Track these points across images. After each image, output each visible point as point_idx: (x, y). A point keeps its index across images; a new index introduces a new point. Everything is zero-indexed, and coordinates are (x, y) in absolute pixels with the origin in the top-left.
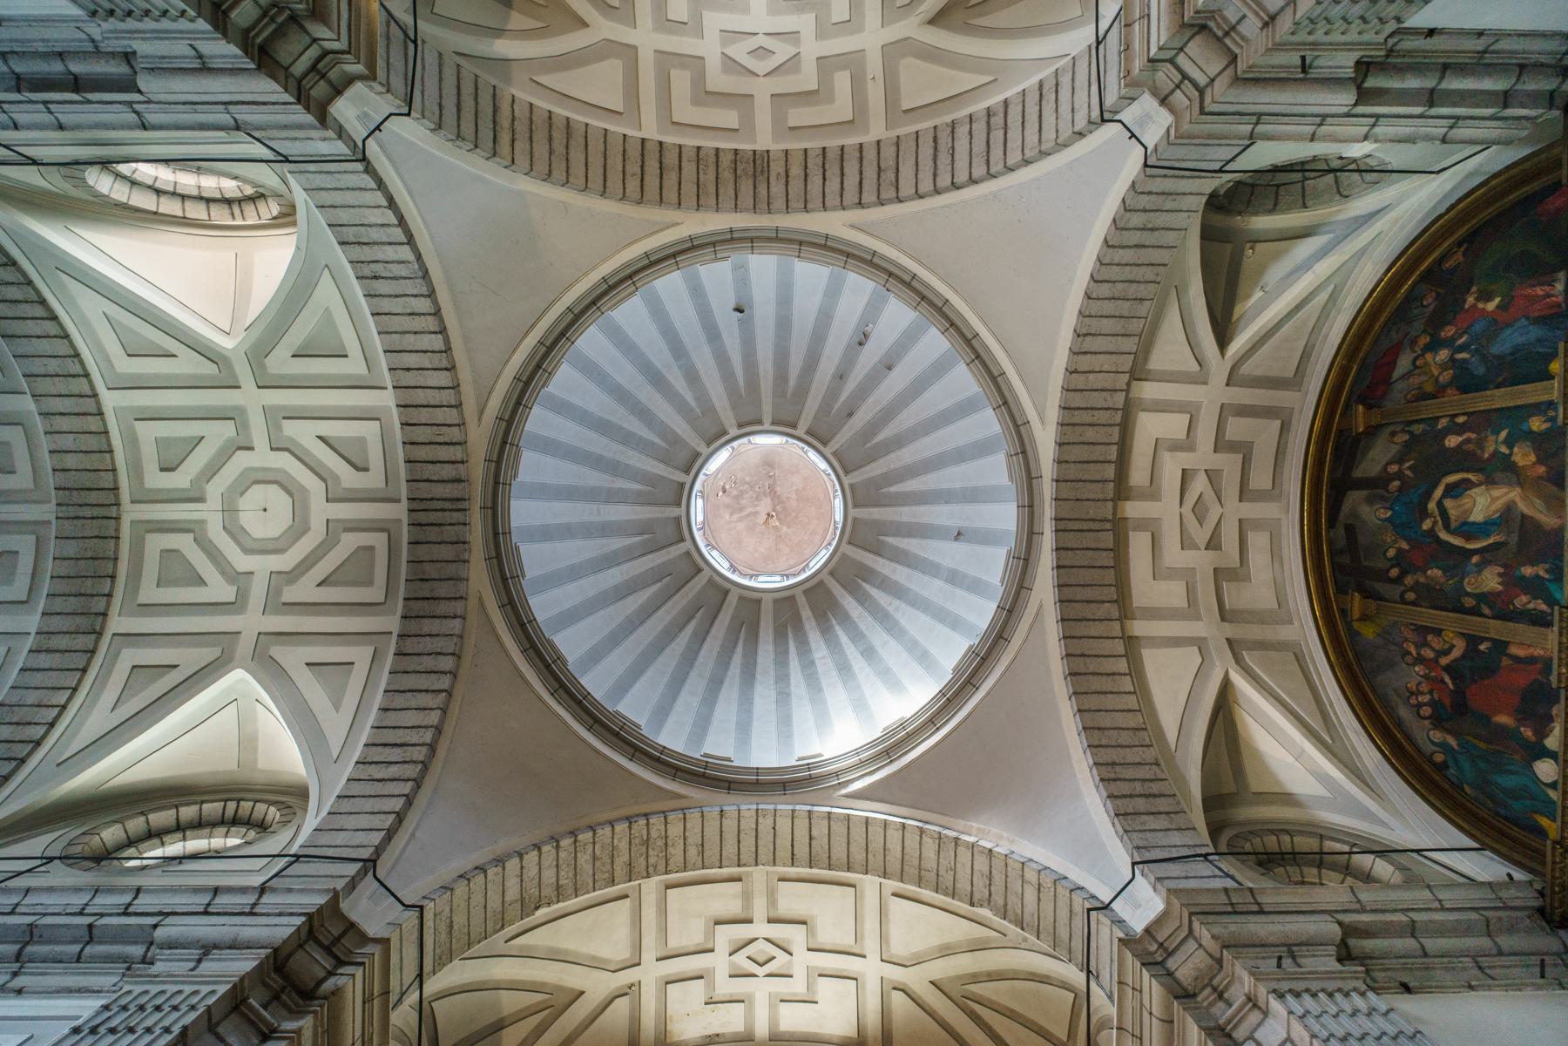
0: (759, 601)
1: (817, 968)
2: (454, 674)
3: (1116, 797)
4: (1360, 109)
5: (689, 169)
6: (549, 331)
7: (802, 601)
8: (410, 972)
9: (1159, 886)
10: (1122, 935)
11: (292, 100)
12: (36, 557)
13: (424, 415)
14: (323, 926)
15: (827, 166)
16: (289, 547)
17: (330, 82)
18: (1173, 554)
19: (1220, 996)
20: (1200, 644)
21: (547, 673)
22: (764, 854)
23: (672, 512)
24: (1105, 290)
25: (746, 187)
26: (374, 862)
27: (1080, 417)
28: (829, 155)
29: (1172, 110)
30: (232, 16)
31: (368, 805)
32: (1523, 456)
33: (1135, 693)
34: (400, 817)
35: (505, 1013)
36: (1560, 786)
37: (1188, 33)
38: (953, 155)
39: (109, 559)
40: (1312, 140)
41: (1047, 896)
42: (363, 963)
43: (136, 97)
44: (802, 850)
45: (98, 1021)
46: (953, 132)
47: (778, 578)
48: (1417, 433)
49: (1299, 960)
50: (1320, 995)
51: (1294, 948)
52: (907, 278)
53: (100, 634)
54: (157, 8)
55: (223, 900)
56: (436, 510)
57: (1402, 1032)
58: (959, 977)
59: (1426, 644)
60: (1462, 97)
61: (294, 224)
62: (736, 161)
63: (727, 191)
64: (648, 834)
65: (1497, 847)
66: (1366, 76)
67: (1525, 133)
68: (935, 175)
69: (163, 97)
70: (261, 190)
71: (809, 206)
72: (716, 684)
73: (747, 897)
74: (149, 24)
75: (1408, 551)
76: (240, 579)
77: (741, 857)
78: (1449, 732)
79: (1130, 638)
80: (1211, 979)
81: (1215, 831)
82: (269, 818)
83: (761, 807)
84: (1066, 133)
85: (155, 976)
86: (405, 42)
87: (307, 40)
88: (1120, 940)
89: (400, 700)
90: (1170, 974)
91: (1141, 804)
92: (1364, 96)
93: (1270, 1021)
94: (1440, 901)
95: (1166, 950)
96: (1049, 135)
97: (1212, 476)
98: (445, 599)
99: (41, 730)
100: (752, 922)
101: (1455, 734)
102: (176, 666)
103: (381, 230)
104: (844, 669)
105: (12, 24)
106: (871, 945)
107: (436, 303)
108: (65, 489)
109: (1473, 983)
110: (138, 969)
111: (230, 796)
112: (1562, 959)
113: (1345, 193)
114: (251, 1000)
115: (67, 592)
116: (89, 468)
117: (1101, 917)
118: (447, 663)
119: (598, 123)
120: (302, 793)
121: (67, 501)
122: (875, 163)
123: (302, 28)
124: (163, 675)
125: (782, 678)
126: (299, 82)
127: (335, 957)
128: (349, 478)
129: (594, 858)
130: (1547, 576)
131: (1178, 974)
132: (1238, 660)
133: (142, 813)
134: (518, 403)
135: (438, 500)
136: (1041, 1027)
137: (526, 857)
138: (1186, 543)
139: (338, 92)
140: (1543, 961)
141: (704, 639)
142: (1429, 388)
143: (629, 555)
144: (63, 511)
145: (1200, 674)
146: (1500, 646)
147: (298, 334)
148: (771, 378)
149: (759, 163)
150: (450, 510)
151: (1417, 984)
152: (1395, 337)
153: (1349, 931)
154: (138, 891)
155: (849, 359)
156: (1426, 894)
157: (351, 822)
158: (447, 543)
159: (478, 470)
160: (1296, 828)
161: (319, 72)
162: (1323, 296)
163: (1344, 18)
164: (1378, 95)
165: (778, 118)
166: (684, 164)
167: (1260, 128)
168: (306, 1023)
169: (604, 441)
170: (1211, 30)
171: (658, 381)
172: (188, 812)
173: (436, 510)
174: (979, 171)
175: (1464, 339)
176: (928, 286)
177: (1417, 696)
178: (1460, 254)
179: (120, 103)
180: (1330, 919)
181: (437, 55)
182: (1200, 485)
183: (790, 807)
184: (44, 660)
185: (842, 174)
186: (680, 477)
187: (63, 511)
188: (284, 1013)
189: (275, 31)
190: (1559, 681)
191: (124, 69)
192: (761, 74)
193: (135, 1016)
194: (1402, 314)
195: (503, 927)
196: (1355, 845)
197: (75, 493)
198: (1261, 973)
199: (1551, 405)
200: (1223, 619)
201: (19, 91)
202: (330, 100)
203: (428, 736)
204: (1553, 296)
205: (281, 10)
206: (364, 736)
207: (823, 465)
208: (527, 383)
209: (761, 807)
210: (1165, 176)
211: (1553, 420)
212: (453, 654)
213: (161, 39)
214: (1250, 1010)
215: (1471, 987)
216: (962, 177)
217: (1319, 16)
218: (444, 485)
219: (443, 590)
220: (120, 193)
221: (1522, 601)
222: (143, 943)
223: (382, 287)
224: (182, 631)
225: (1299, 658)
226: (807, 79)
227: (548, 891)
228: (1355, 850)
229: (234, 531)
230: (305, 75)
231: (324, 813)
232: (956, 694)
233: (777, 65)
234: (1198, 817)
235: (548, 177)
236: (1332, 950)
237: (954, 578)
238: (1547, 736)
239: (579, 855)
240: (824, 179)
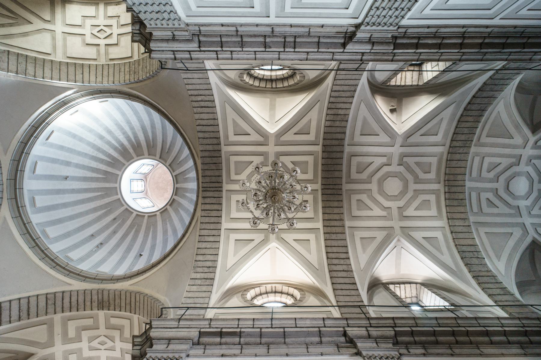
1: (82, 28)
5: (123, 304)
13: (213, 220)
15: (77, 305)
22: (100, 69)
25: (106, 298)
28: (76, 309)
38: (20, 309)
44: (86, 70)
52: (58, 267)
56: (212, 187)
62: (109, 307)
64: (134, 76)
71: (83, 292)
73: (107, 53)
77: (108, 67)
98: (207, 157)
100: (105, 45)
102: (295, 134)
105: (217, 355)
106: (59, 37)
108: (339, 194)
115: (336, 159)
116: (330, 202)
121: (338, 190)
124: (299, 131)
128: (364, 197)
129: (146, 67)
135: (212, 191)
144: (340, 187)
149: (101, 306)
150: (207, 187)
158: (208, 176)
166: (124, 306)
173: (212, 187)
185: (70, 302)
187: (340, 187)
192: (102, 336)
197: (335, 193)
218: (209, 196)
224: (296, 146)
226: (85, 335)
233: (97, 339)
240: (77, 301)
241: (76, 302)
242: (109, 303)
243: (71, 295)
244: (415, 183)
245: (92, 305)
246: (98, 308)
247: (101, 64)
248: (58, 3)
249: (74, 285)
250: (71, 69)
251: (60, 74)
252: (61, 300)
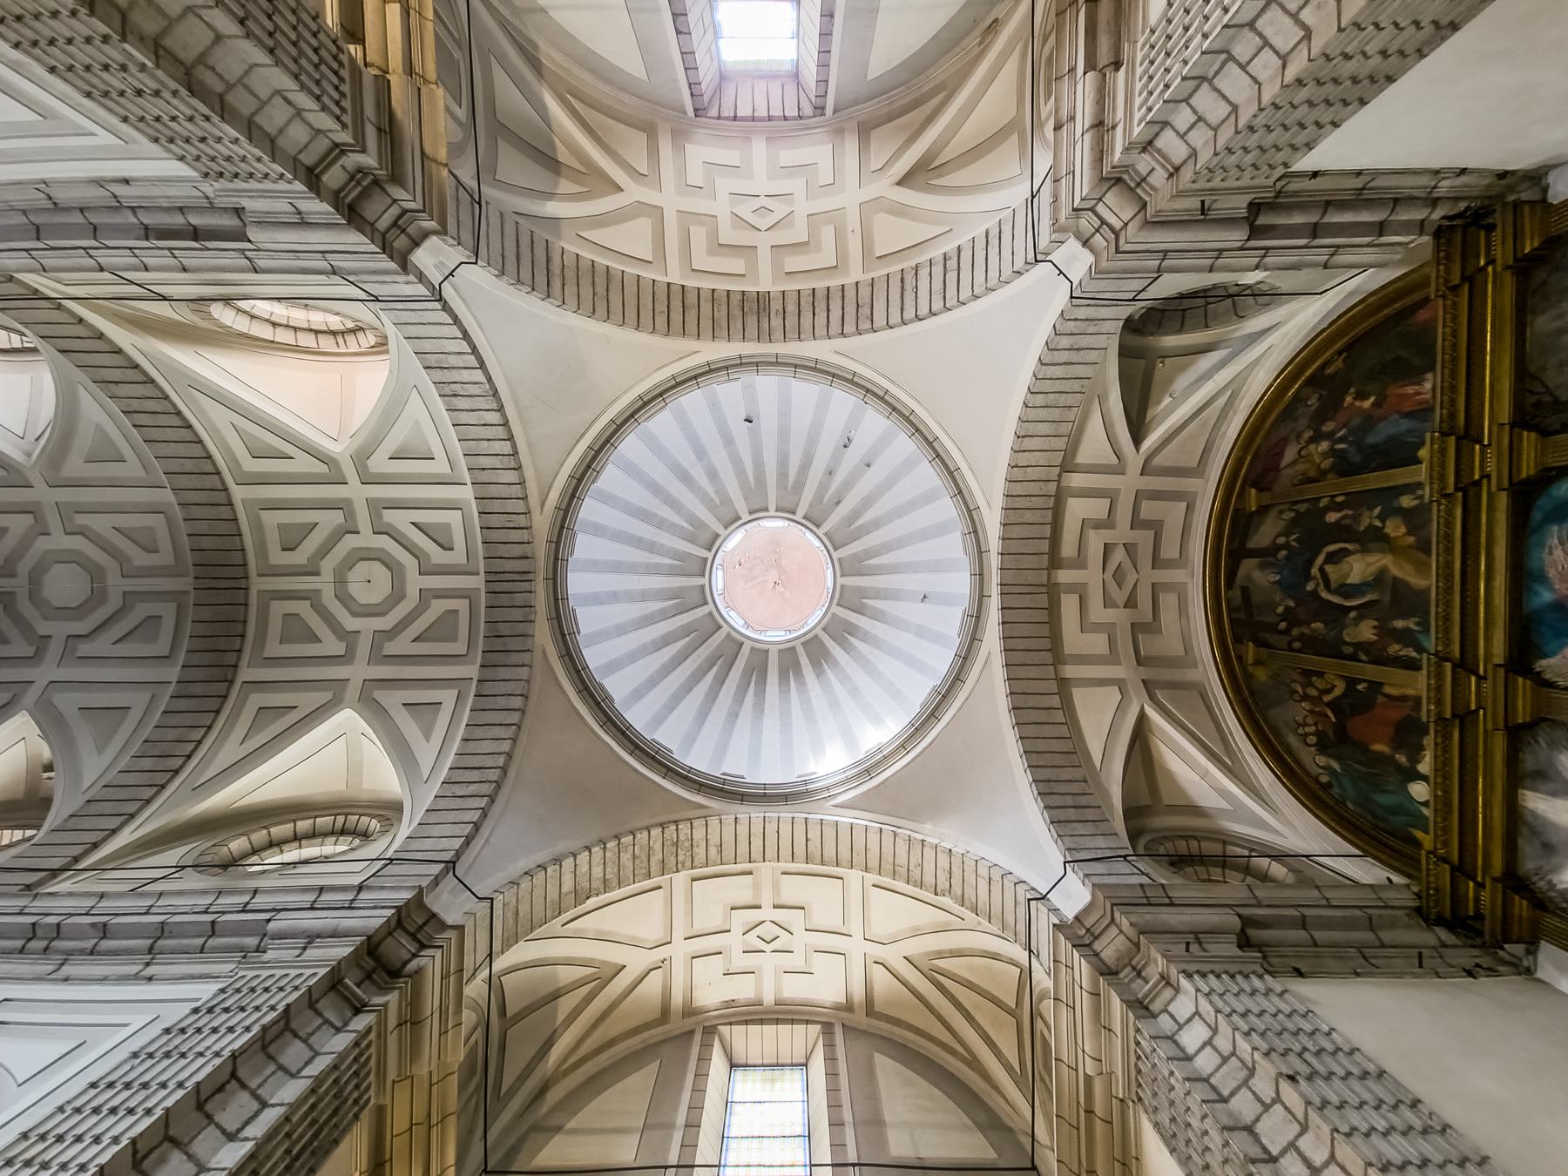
0: (767, 651)
2: (523, 711)
3: (1051, 808)
4: (1252, 243)
5: (706, 307)
6: (597, 438)
7: (801, 651)
8: (482, 952)
9: (1086, 881)
10: (1057, 922)
11: (379, 250)
12: (177, 620)
14: (409, 916)
16: (390, 611)
17: (409, 236)
18: (1098, 613)
19: (1139, 974)
20: (1120, 684)
21: (597, 709)
22: (771, 852)
23: (698, 581)
24: (1040, 400)
25: (752, 322)
26: (454, 863)
27: (1020, 503)
29: (1092, 251)
30: (324, 179)
31: (452, 817)
32: (1395, 528)
33: (1066, 723)
34: (477, 826)
35: (561, 985)
36: (1432, 804)
37: (1106, 185)
39: (239, 621)
40: (1210, 271)
41: (996, 888)
42: (442, 946)
43: (247, 245)
44: (800, 850)
45: (214, 1002)
46: (916, 274)
47: (783, 633)
48: (1302, 511)
49: (1205, 946)
50: (1223, 976)
51: (1200, 936)
52: (881, 393)
53: (232, 682)
54: (259, 172)
55: (327, 897)
57: (1295, 1011)
58: (927, 954)
59: (1311, 685)
60: (1341, 229)
61: (387, 352)
63: (737, 325)
65: (1379, 855)
66: (1257, 215)
67: (1398, 257)
68: (902, 310)
69: (269, 246)
70: (360, 324)
71: (802, 337)
72: (734, 715)
73: (757, 887)
74: (253, 185)
75: (1294, 608)
76: (348, 637)
78: (1331, 756)
79: (1062, 679)
80: (1131, 960)
81: (1133, 836)
82: (372, 828)
83: (767, 815)
84: (1007, 272)
85: (266, 963)
86: (472, 203)
87: (389, 201)
88: (1054, 925)
89: (479, 733)
90: (1097, 955)
91: (1071, 814)
92: (1256, 232)
93: (1181, 998)
94: (1327, 899)
95: (1092, 934)
96: (994, 274)
97: (1130, 548)
99: (180, 761)
101: (1338, 759)
102: (296, 707)
103: (458, 357)
104: (834, 704)
106: (855, 927)
107: (504, 416)
109: (1359, 971)
110: (253, 957)
111: (339, 811)
112: (1438, 953)
113: (1241, 315)
114: (346, 980)
117: (1040, 906)
118: (517, 702)
119: (632, 270)
120: (397, 807)
122: (855, 300)
123: (384, 190)
125: (785, 712)
126: (384, 235)
127: (419, 941)
128: (141, 559)
129: (634, 857)
130: (1416, 628)
131: (1103, 955)
132: (1152, 697)
133: (265, 827)
134: (573, 496)
136: (993, 996)
137: (579, 857)
138: (1108, 602)
139: (416, 244)
140: (1420, 953)
141: (723, 682)
142: (1312, 474)
143: (664, 615)
145: (1121, 708)
146: (1376, 687)
147: (391, 444)
148: (775, 475)
149: (759, 304)
151: (1307, 969)
152: (1283, 431)
153: (1247, 922)
154: (256, 892)
155: (836, 459)
156: (1315, 893)
157: (437, 831)
159: (541, 550)
160: (1204, 834)
161: (399, 227)
162: (1223, 400)
163: (1238, 167)
164: (1268, 231)
165: (777, 265)
167: (1167, 263)
168: (392, 998)
169: (644, 525)
170: (1125, 182)
171: (686, 478)
172: (304, 825)
174: (937, 305)
175: (1341, 433)
176: (897, 400)
177: (1304, 727)
178: (1340, 361)
179: (233, 250)
180: (1230, 911)
181: (499, 214)
182: (1119, 556)
183: (791, 815)
184: (182, 704)
185: (828, 310)
186: (704, 553)
188: (373, 989)
189: (361, 193)
190: (1429, 716)
191: (235, 222)
193: (193, 1038)
194: (1289, 413)
195: (560, 914)
196: (1253, 850)
198: (1172, 956)
199: (1420, 485)
200: (1139, 662)
201: (147, 240)
202: (410, 251)
203: (501, 761)
204: (1421, 394)
205: (366, 175)
206: (450, 761)
207: (817, 543)
208: (580, 480)
209: (767, 815)
210: (1088, 305)
211: (1421, 497)
212: (522, 695)
213: (265, 197)
214: (1164, 987)
215: (1358, 975)
216: (923, 311)
217: (1217, 165)
219: (514, 644)
220: (241, 324)
221: (1394, 649)
222: (257, 935)
223: (461, 403)
225: (1204, 697)
226: (799, 234)
227: (596, 884)
228: (1253, 854)
229: (344, 598)
230: (388, 230)
231: (415, 824)
232: (923, 724)
234: (1119, 824)
235: (593, 314)
236: (1233, 938)
237: (922, 632)
238: (1420, 762)
239: (622, 854)
240: (814, 314)
244: (12, 594)
247: (767, 863)
248: (860, 1004)
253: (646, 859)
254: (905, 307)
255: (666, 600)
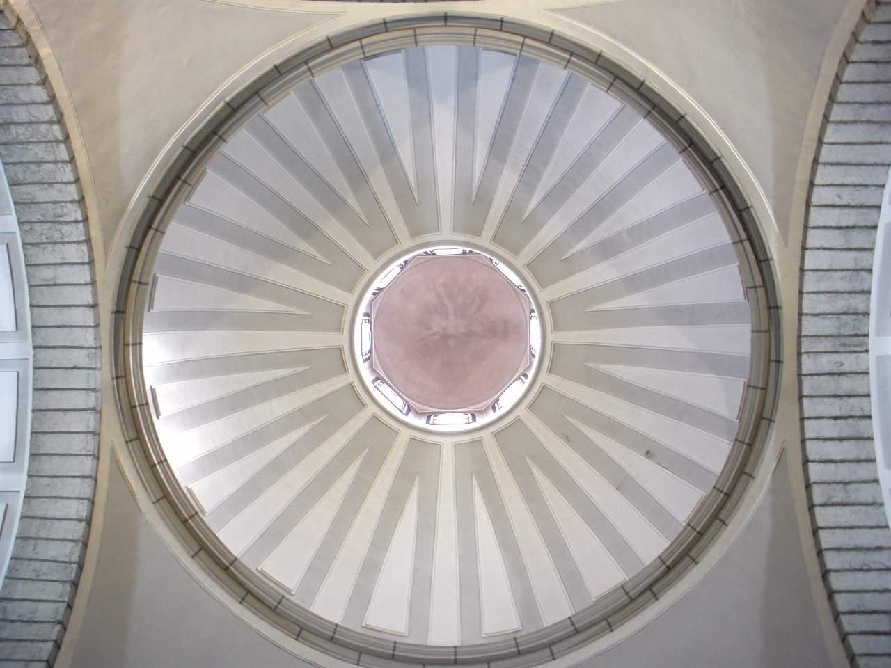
15: (850, 421)
28: (864, 422)
44: (53, 400)
47: (367, 348)
62: (857, 314)
129: (39, 163)
185: (841, 439)
239: (43, 145)
240: (836, 418)
241: (842, 422)
242: (845, 313)
243: (817, 439)
245: (851, 373)
246: (861, 352)
249: (785, 441)
250: (47, 466)
251: (67, 477)
252: (833, 465)
253: (36, 179)
254: (843, 553)
255: (417, 176)
